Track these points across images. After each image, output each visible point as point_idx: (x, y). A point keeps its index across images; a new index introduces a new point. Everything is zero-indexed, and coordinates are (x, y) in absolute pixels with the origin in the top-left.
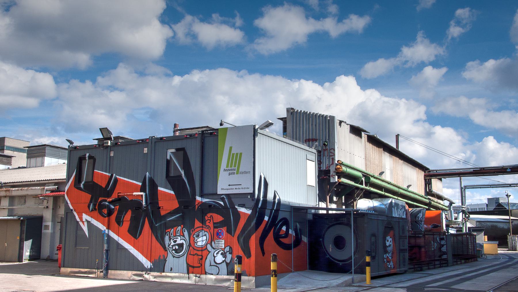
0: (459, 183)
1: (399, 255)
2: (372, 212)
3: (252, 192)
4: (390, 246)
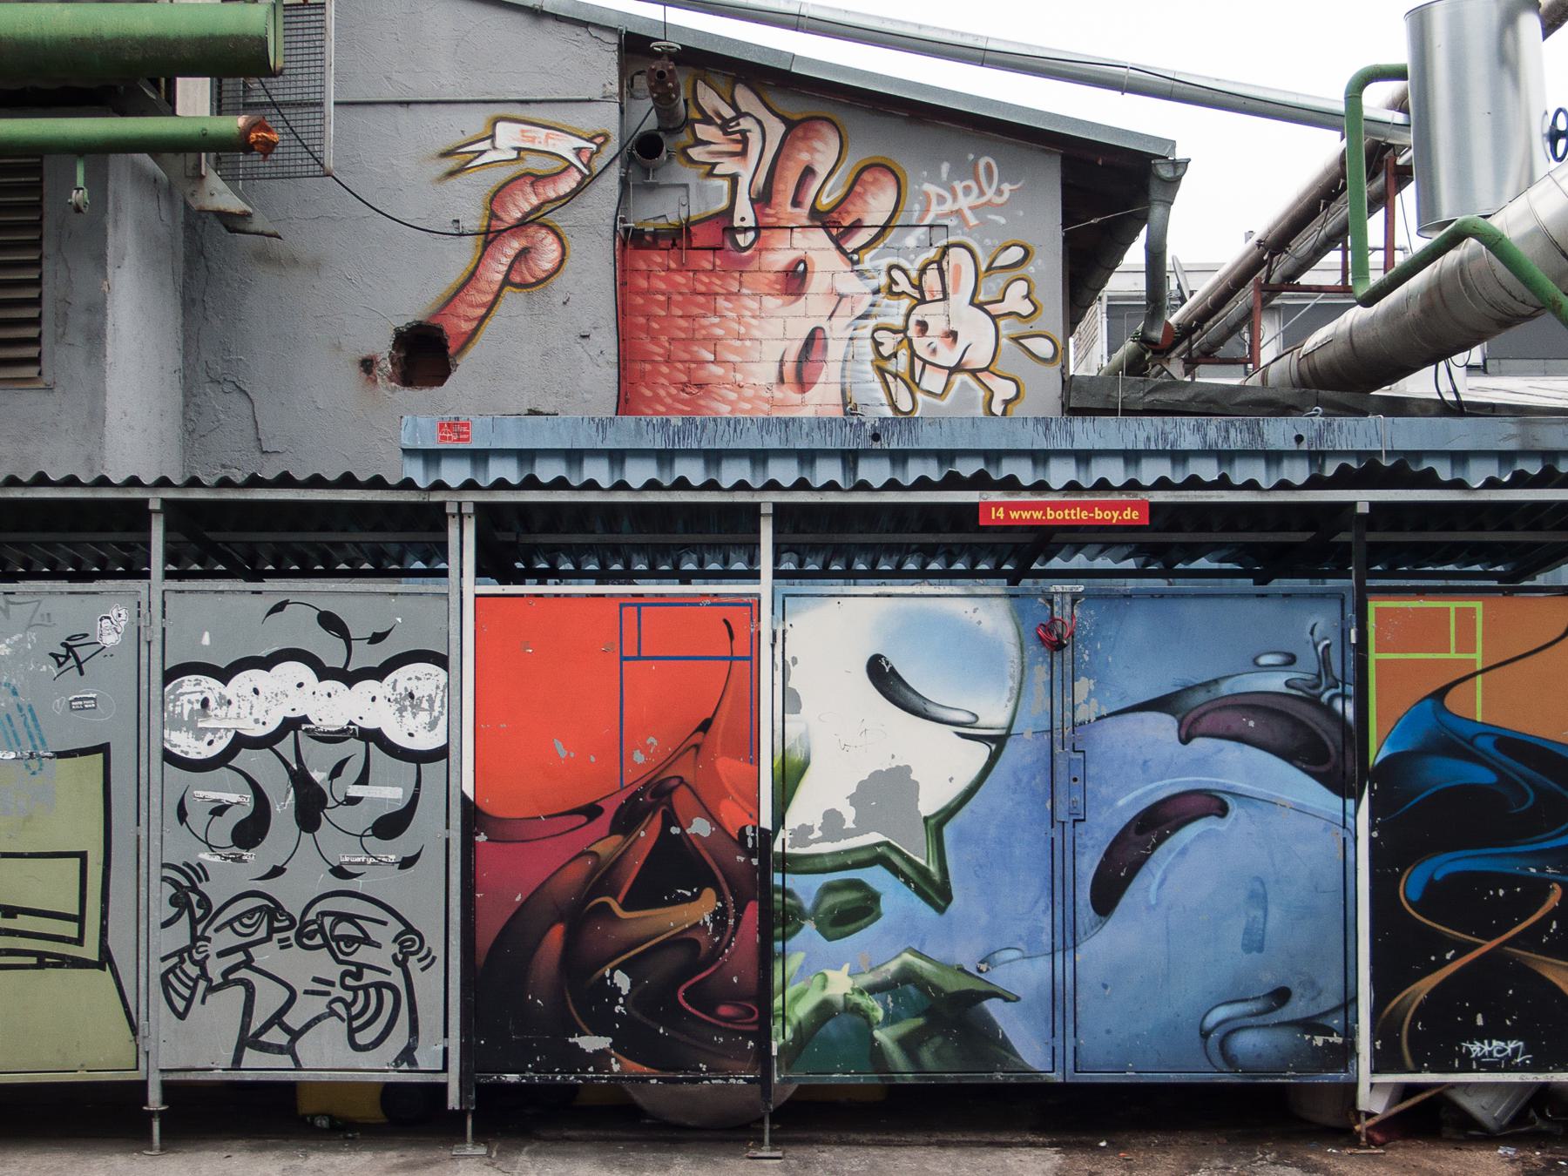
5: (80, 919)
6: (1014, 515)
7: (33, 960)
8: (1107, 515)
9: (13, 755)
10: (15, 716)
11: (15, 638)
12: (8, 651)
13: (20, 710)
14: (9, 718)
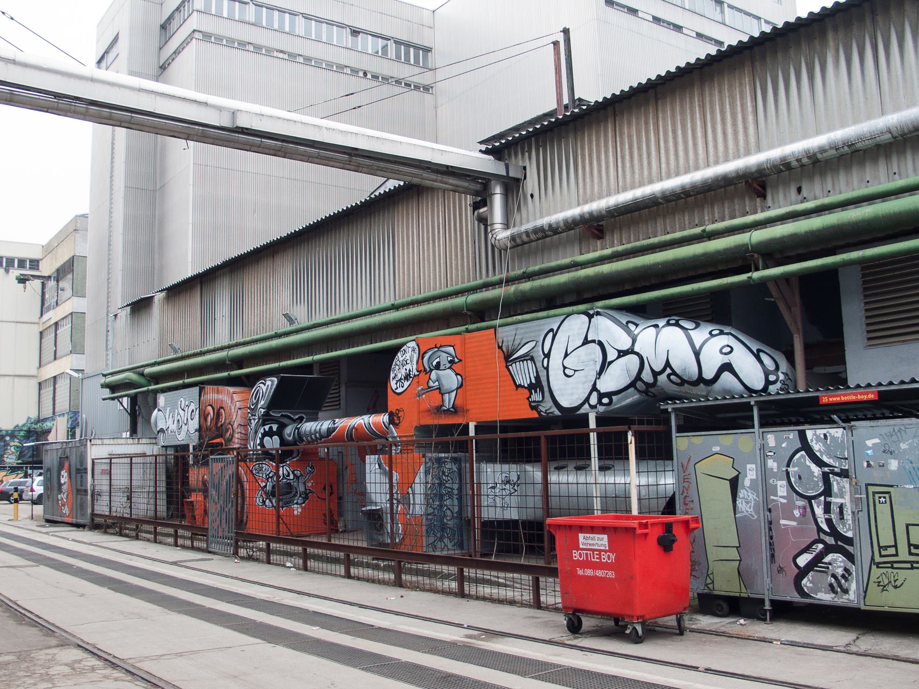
0: (715, 587)
1: (76, 498)
2: (828, 400)
3: (798, 571)
4: (64, 484)
5: (895, 546)
6: (831, 399)
7: (895, 565)
8: (862, 397)
9: (913, 487)
10: (912, 471)
11: (910, 441)
12: (907, 447)
13: (914, 469)
14: (910, 472)
